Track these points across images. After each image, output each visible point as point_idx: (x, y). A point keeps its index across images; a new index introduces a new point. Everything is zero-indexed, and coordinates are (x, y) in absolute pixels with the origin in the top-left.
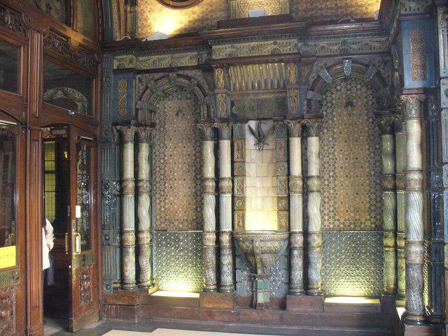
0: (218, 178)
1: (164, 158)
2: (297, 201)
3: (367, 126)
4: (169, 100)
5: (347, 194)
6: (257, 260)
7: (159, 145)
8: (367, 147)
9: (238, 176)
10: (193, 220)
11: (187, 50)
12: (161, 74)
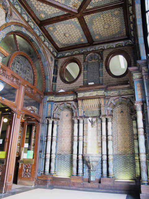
6: (91, 164)
11: (70, 95)
12: (62, 103)
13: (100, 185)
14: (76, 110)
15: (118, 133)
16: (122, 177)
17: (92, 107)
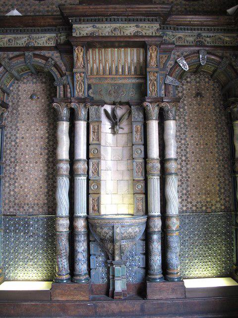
0: (72, 160)
1: (15, 141)
2: (155, 183)
3: (215, 115)
4: (24, 83)
5: (198, 177)
6: (116, 247)
7: (11, 127)
8: (215, 134)
9: (93, 158)
10: (44, 204)
11: (45, 31)
12: (17, 53)
13: (147, 305)
14: (64, 78)
15: (187, 153)
16: (197, 272)
17: (114, 72)
